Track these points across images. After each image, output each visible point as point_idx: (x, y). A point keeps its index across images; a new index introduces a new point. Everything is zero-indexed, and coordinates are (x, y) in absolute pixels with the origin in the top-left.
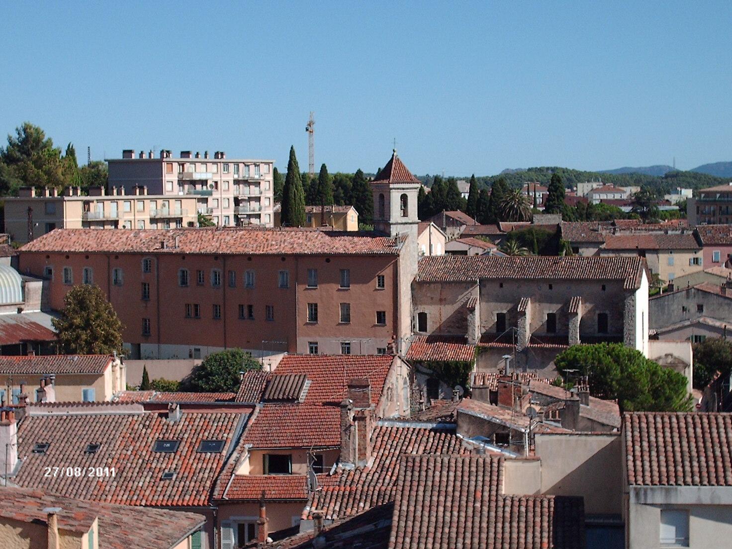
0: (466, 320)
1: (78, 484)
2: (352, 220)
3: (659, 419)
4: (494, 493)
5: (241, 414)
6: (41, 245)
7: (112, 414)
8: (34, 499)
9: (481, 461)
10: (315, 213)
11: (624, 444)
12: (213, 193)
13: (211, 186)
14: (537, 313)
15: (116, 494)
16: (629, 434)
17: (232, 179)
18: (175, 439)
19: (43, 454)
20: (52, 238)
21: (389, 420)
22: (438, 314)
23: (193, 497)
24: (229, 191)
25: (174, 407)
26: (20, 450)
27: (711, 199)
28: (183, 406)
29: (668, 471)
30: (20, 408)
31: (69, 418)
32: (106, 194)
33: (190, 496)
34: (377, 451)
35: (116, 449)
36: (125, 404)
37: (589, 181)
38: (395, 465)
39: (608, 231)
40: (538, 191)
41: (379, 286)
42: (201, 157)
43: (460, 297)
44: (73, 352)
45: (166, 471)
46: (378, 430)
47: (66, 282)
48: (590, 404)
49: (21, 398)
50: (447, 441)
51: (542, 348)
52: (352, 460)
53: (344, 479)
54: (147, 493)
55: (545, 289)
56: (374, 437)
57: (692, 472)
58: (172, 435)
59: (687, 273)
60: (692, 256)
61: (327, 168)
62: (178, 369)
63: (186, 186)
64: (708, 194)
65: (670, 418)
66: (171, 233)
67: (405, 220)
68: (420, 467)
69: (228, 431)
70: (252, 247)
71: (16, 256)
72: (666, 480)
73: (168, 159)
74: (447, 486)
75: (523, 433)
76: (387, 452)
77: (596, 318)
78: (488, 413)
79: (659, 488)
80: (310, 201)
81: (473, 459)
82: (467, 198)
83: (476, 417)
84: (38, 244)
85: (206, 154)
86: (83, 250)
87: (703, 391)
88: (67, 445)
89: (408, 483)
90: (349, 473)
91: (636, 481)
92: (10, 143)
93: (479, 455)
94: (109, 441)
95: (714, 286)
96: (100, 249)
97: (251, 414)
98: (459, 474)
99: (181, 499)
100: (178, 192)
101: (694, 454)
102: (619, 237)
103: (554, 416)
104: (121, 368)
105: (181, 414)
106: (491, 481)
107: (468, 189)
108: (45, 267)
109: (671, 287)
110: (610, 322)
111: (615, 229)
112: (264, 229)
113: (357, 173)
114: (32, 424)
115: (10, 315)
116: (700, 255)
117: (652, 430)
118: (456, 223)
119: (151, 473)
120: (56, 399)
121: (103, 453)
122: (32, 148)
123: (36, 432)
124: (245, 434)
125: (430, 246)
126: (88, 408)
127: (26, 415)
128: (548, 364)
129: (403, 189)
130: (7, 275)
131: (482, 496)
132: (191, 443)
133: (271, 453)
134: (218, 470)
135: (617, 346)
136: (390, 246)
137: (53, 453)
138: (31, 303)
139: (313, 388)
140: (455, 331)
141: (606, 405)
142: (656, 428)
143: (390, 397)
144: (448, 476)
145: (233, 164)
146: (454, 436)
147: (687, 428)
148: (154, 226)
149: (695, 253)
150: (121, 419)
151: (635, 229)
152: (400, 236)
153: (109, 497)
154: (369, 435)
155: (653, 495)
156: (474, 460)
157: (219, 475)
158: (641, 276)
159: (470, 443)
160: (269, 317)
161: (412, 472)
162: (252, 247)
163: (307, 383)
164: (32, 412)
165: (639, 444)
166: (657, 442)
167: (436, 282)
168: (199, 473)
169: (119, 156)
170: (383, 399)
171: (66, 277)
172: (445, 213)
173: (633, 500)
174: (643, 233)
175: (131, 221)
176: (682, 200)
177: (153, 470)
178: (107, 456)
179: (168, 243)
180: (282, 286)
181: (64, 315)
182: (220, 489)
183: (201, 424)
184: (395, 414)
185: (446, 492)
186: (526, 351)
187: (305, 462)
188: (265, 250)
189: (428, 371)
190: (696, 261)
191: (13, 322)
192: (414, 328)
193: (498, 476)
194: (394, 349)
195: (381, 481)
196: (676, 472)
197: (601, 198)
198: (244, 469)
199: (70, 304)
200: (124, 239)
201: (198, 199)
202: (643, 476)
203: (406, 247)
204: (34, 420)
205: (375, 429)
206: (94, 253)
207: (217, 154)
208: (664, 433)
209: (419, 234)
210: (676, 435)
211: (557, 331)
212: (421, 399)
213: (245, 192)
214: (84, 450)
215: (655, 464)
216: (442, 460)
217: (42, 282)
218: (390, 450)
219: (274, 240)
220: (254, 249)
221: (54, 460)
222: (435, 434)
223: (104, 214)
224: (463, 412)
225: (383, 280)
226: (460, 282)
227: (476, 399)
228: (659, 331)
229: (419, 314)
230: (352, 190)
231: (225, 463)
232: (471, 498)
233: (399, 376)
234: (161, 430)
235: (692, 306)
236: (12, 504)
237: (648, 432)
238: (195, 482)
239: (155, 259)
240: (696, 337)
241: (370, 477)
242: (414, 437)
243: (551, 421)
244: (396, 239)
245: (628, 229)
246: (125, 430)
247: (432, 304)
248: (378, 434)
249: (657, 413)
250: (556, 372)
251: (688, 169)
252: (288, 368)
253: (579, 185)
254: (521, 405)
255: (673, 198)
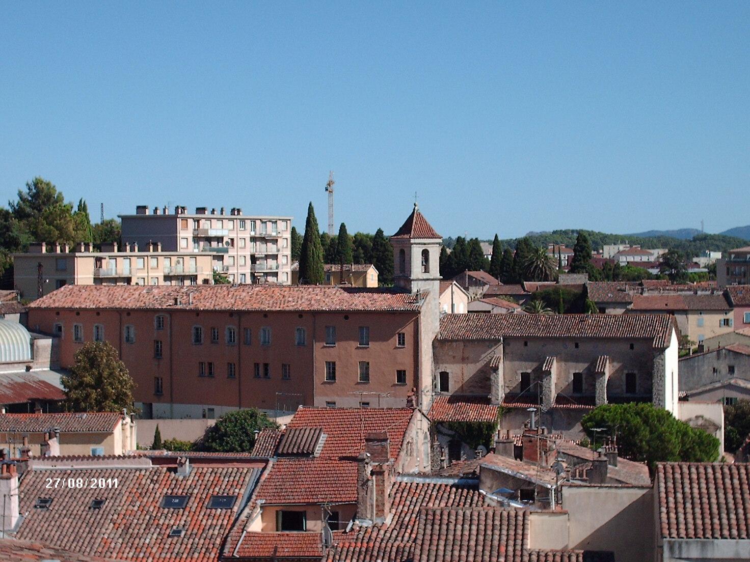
0: (489, 379)
1: (82, 541)
2: (372, 277)
3: (693, 470)
4: (519, 547)
5: (253, 468)
6: (51, 301)
7: (119, 468)
8: (31, 553)
9: (505, 514)
10: (334, 272)
11: (656, 496)
12: (229, 250)
13: (227, 243)
14: (563, 374)
15: (122, 551)
16: (662, 485)
17: (249, 236)
18: (184, 494)
19: (45, 509)
20: (62, 294)
21: (409, 475)
22: (461, 373)
23: (202, 555)
24: (244, 250)
25: (183, 461)
26: (22, 505)
27: (741, 260)
28: (192, 461)
29: (703, 524)
30: (22, 461)
31: (74, 472)
32: (119, 251)
33: (199, 553)
34: (395, 507)
35: (122, 505)
36: (132, 459)
37: (615, 244)
38: (415, 522)
39: (635, 291)
40: (563, 253)
41: (399, 343)
42: (217, 214)
43: (483, 356)
44: (84, 410)
45: (175, 528)
46: (396, 486)
47: (76, 339)
48: (619, 465)
49: (24, 452)
50: (469, 497)
51: (568, 409)
52: (369, 516)
53: (361, 536)
54: (154, 550)
55: (572, 348)
56: (393, 493)
57: (730, 525)
58: (181, 491)
59: (717, 335)
60: (722, 317)
61: (346, 228)
62: (189, 429)
63: (202, 243)
64: (738, 255)
65: (705, 469)
66: (185, 290)
67: (426, 276)
68: (441, 520)
69: (239, 486)
70: (269, 304)
71: (24, 313)
72: (702, 533)
73: (183, 216)
74: (469, 541)
75: (549, 489)
76: (406, 509)
77: (624, 378)
78: (513, 468)
79: (694, 541)
80: (329, 259)
81: (496, 512)
82: (490, 259)
83: (500, 473)
84: (46, 301)
85: (222, 210)
86: (94, 307)
87: (735, 454)
88: (71, 500)
89: (428, 537)
90: (366, 530)
91: (670, 534)
92: (21, 198)
93: (503, 508)
94: (115, 496)
95: (746, 347)
96: (112, 306)
97: (264, 469)
98: (482, 527)
99: (190, 556)
100: (193, 248)
101: (731, 506)
102: (647, 298)
103: (581, 475)
104: (131, 427)
105: (191, 469)
106: (515, 535)
107: (491, 251)
108: (54, 324)
109: (701, 347)
110: (638, 381)
111: (642, 289)
112: (281, 286)
113: (377, 232)
114: (34, 478)
115: (18, 373)
116: (730, 316)
117: (687, 481)
118: (478, 283)
119: (158, 530)
120: (60, 453)
121: (108, 509)
122: (44, 203)
123: (39, 487)
124: (258, 489)
125: (453, 305)
126: (93, 462)
127: (29, 469)
128: (574, 425)
129: (425, 244)
130: (14, 331)
131: (506, 551)
132: (200, 498)
133: (285, 509)
134: (229, 526)
135: (646, 406)
136: (411, 303)
137: (56, 508)
138: (40, 361)
139: (330, 442)
140: (478, 391)
141: (635, 466)
142: (690, 479)
143: (409, 452)
144: (470, 530)
145: (249, 221)
146: (476, 492)
147: (723, 479)
148: (168, 283)
149: (726, 314)
150: (127, 474)
151: (663, 290)
152: (421, 292)
153: (114, 555)
154: (388, 492)
155: (688, 548)
156: (498, 513)
157: (229, 532)
158: (670, 335)
159: (493, 499)
160: (286, 376)
161: (433, 525)
162: (269, 304)
163: (323, 437)
164: (35, 466)
165: (673, 496)
166: (692, 493)
167: (458, 340)
168: (209, 530)
169: (133, 212)
170: (403, 454)
171: (77, 334)
172: (468, 273)
173: (666, 554)
174: (672, 294)
175: (144, 279)
176: (711, 263)
177: (160, 527)
178: (112, 512)
179: (181, 300)
180: (298, 344)
181: (74, 373)
182: (230, 546)
183: (212, 479)
184: (416, 470)
185: (468, 546)
186: (551, 412)
187: (320, 519)
188: (281, 306)
189: (450, 432)
190: (726, 322)
191: (21, 380)
192: (435, 387)
193: (523, 530)
194: (414, 402)
195: (400, 538)
196: (712, 524)
197: (628, 260)
198: (256, 525)
199: (80, 361)
200: (136, 296)
201: (213, 256)
202: (678, 529)
203: (428, 303)
204: (37, 475)
205: (394, 485)
206: (105, 309)
207: (233, 210)
208: (699, 484)
209: (441, 293)
210: (712, 486)
211: (584, 391)
212: (442, 456)
213: (262, 249)
214: (89, 506)
215: (690, 517)
216: (464, 513)
217: (51, 340)
218: (409, 506)
219: (291, 296)
220: (270, 306)
221: (57, 516)
222: (457, 490)
223: (116, 271)
224: (486, 467)
225: (404, 337)
226: (484, 340)
227: (499, 454)
228: (689, 393)
229: (440, 373)
230: (373, 250)
231: (236, 520)
232: (495, 553)
233: (419, 430)
234: (170, 485)
235: (723, 367)
236: (8, 557)
237: (682, 483)
238: (205, 540)
239: (168, 316)
240: (727, 399)
241: (388, 535)
242: (434, 493)
243: (579, 480)
244: (417, 295)
245: (657, 289)
246: (131, 486)
247: (453, 363)
248: (397, 490)
249: (692, 463)
250: (582, 434)
251: (717, 233)
252: (303, 422)
253: (605, 247)
254: (547, 461)
255: (702, 261)
